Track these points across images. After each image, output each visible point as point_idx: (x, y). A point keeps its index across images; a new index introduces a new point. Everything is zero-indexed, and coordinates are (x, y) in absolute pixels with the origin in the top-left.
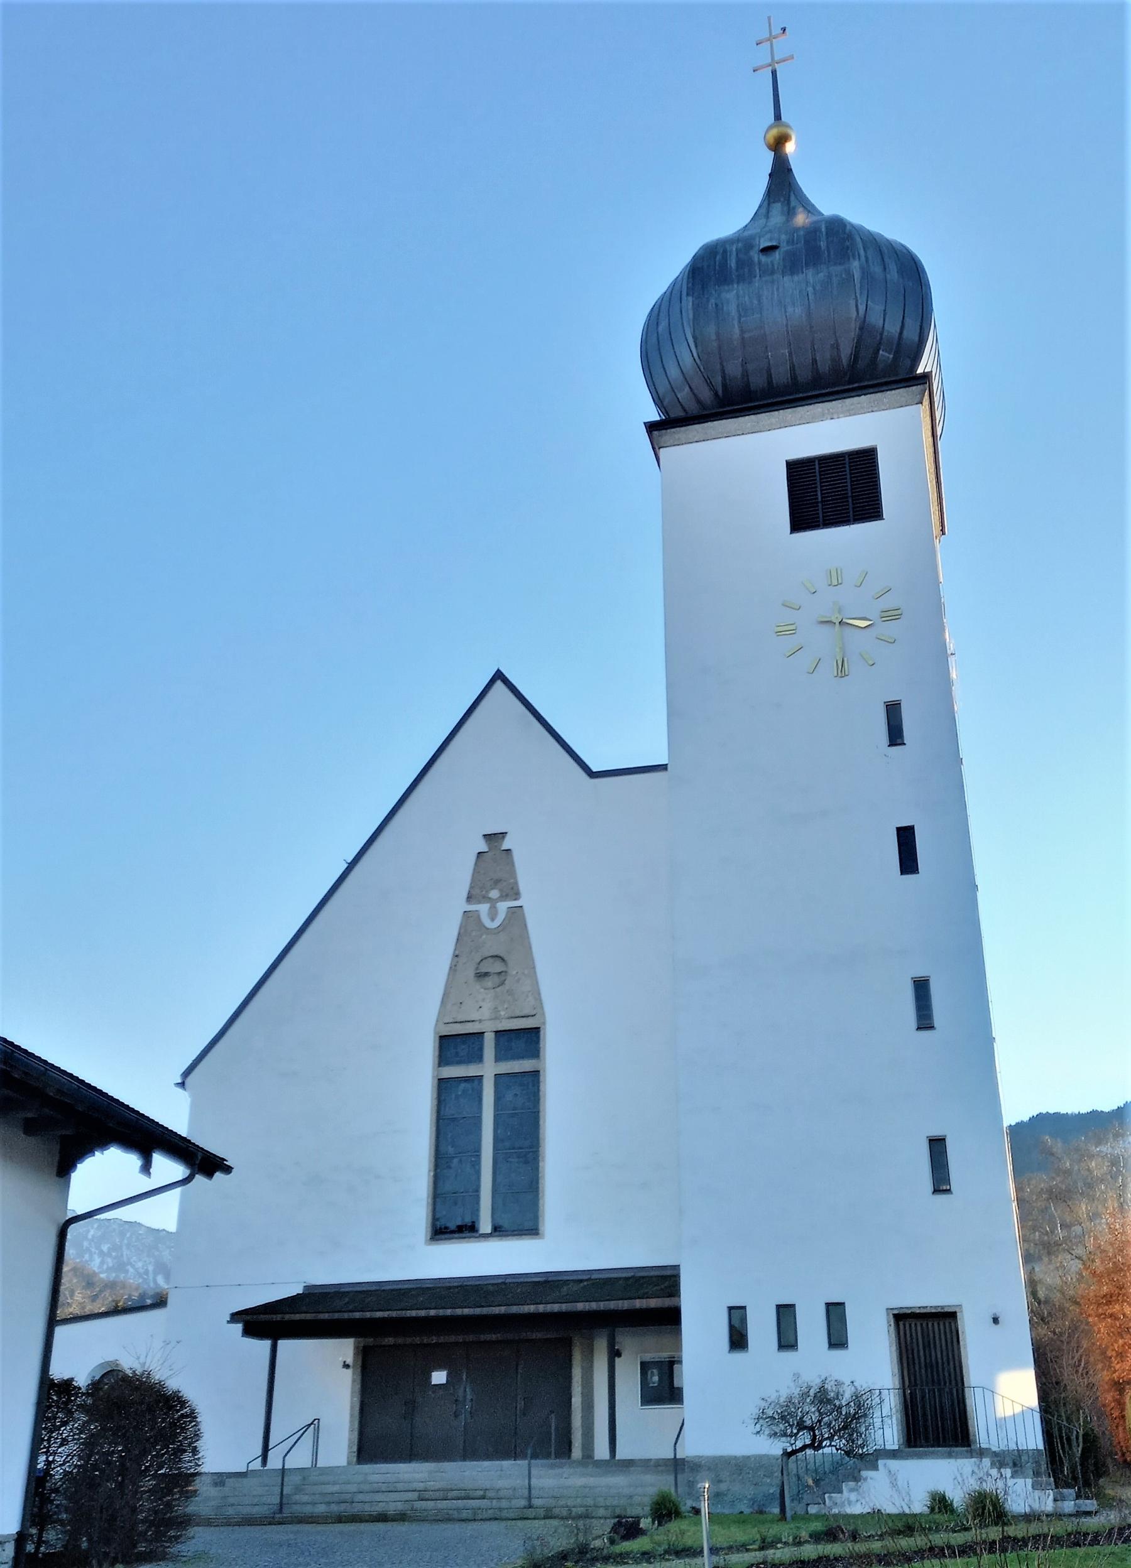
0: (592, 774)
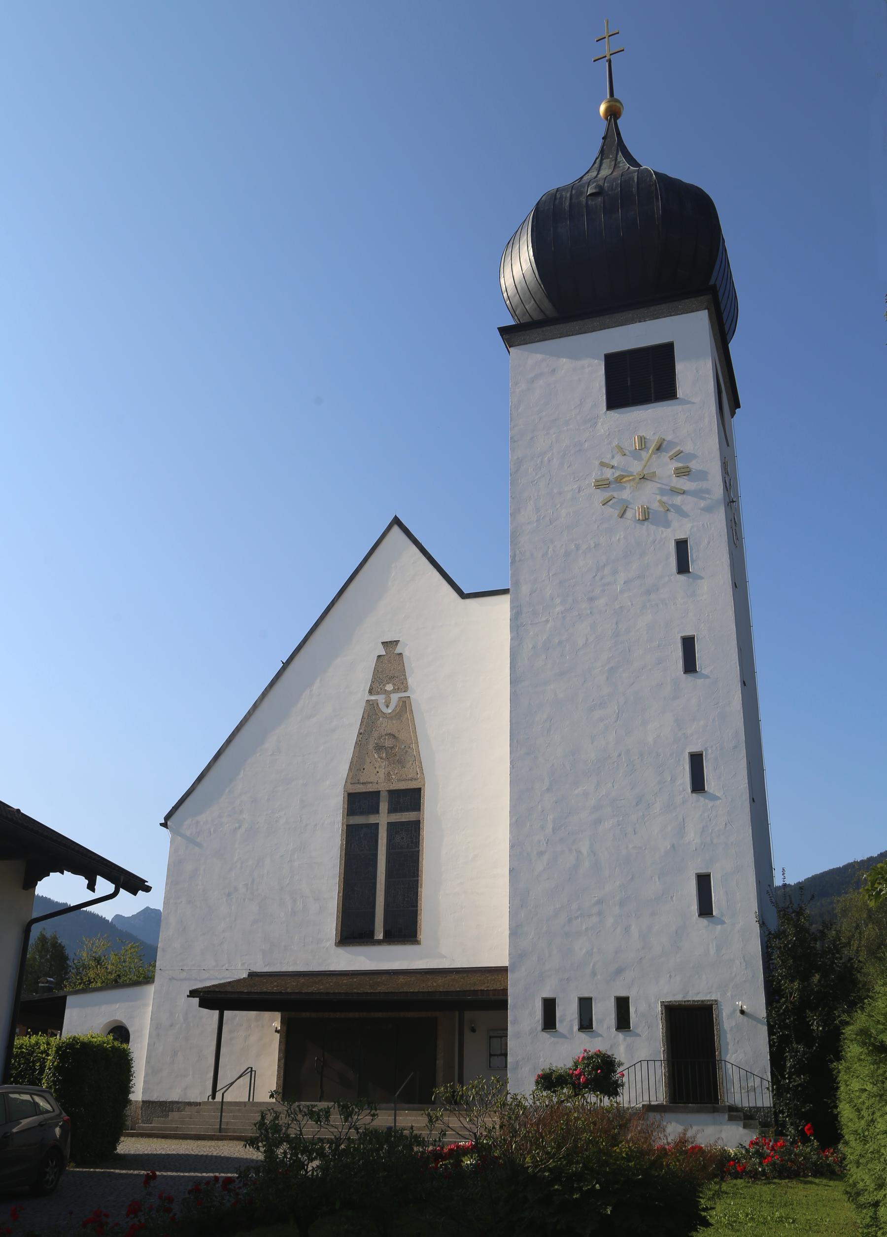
0: (463, 596)
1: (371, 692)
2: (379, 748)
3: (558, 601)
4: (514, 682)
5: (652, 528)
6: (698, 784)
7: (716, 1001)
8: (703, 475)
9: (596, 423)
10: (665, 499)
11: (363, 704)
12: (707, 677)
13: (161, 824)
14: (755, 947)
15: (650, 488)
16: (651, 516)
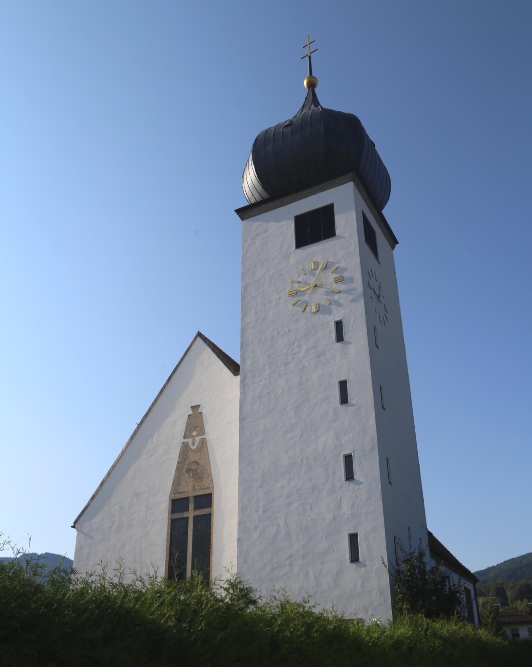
1: (185, 437)
2: (188, 471)
3: (267, 367)
4: (242, 420)
5: (321, 316)
6: (349, 476)
7: (361, 619)
8: (351, 280)
9: (289, 258)
10: (329, 297)
11: (180, 445)
12: (354, 405)
13: (72, 527)
14: (386, 580)
15: (320, 292)
16: (320, 309)
